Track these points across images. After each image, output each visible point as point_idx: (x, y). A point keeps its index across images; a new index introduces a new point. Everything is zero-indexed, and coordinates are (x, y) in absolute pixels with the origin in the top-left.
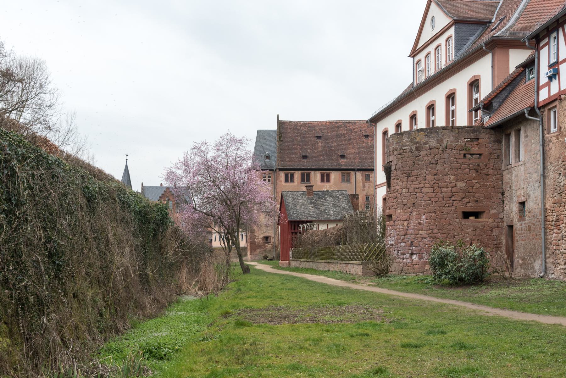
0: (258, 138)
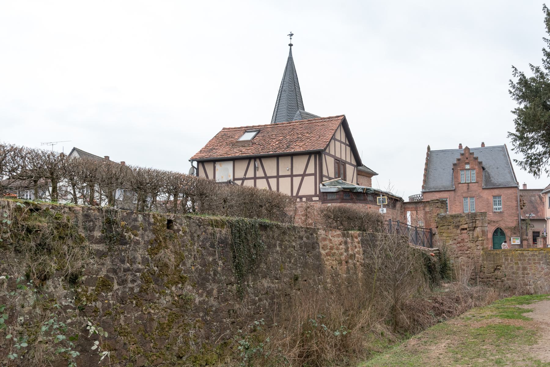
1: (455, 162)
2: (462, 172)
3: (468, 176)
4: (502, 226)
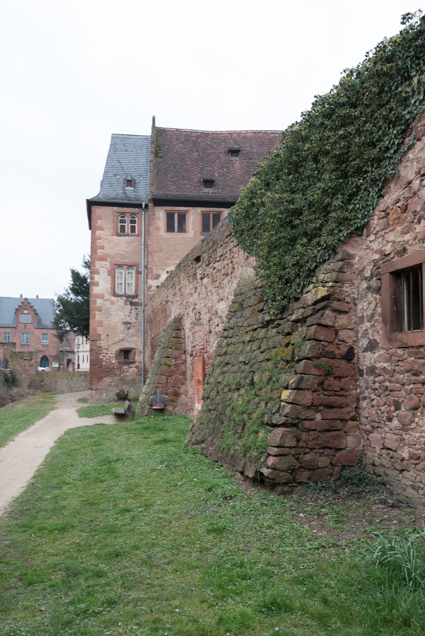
0: (114, 147)
1: (17, 307)
2: (23, 315)
3: (26, 318)
4: (47, 354)
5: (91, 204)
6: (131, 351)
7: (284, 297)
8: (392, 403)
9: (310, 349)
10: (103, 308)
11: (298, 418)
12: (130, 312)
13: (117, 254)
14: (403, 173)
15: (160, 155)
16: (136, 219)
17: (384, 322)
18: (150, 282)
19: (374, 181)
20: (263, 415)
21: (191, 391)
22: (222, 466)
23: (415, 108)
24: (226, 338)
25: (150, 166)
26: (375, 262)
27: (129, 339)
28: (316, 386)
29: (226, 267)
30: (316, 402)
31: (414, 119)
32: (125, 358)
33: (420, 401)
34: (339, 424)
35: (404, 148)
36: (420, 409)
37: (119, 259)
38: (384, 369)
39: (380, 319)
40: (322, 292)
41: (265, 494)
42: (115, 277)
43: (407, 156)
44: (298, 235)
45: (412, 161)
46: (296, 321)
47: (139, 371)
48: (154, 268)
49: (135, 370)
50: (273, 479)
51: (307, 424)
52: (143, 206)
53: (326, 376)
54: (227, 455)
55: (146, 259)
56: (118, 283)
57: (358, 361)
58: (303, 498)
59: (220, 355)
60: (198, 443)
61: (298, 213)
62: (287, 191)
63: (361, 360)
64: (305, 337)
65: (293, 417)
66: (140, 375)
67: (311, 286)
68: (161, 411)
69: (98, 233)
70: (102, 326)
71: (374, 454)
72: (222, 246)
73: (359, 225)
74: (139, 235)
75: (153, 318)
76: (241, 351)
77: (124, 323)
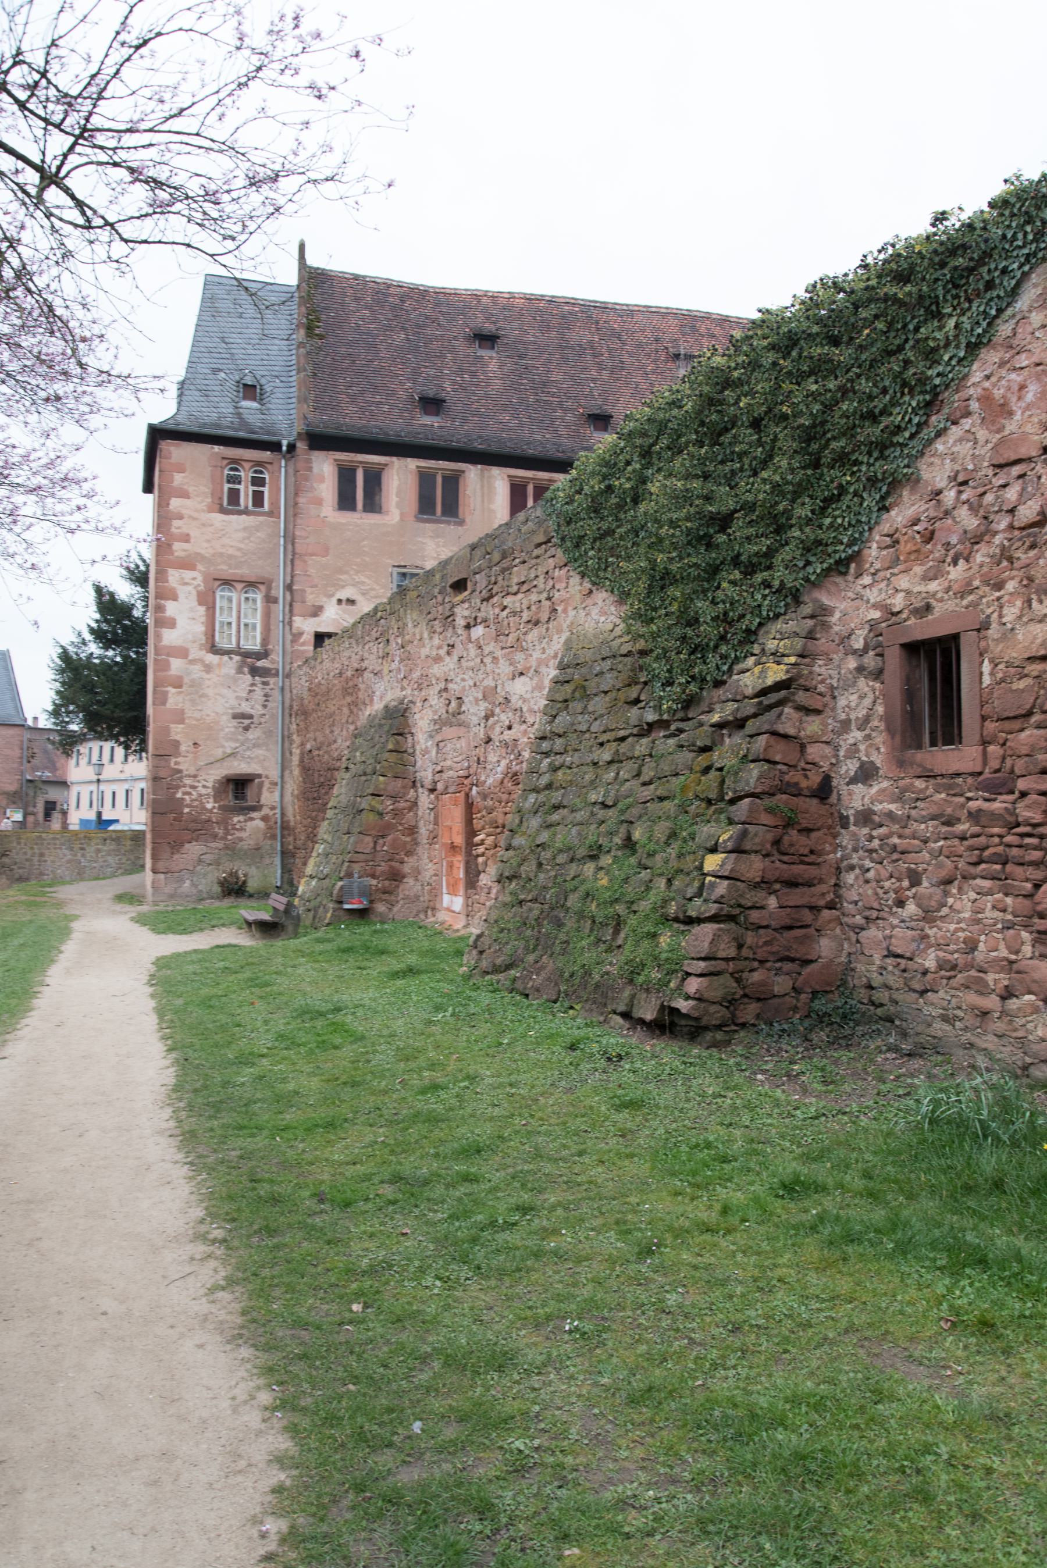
5: (157, 435)
6: (252, 780)
7: (693, 677)
8: (904, 875)
9: (758, 779)
10: (186, 680)
11: (740, 906)
12: (251, 691)
13: (221, 555)
14: (925, 475)
15: (317, 331)
16: (267, 476)
17: (890, 730)
18: (298, 622)
19: (873, 481)
20: (665, 902)
21: (429, 869)
22: (572, 1008)
23: (949, 368)
24: (547, 754)
25: (298, 356)
26: (873, 625)
27: (248, 753)
28: (768, 846)
29: (533, 608)
30: (769, 877)
31: (947, 386)
32: (236, 798)
33: (956, 868)
34: (807, 916)
35: (926, 433)
36: (956, 883)
37: (225, 567)
38: (890, 815)
39: (882, 726)
40: (776, 673)
41: (681, 1048)
42: (214, 607)
43: (933, 447)
44: (722, 563)
45: (942, 456)
46: (720, 726)
47: (270, 828)
48: (309, 590)
49: (261, 824)
50: (697, 1019)
51: (755, 916)
52: (284, 448)
53: (784, 827)
54: (584, 985)
55: (289, 569)
56: (222, 623)
57: (839, 799)
58: (754, 1051)
59: (536, 790)
60: (496, 970)
61: (724, 522)
62: (697, 477)
63: (845, 798)
64: (745, 756)
65: (732, 902)
66: (273, 837)
67: (751, 660)
68: (362, 914)
69: (175, 503)
70: (182, 721)
71: (872, 967)
72: (524, 562)
73: (843, 555)
74: (273, 513)
75: (311, 706)
76: (592, 782)
77: (235, 716)
